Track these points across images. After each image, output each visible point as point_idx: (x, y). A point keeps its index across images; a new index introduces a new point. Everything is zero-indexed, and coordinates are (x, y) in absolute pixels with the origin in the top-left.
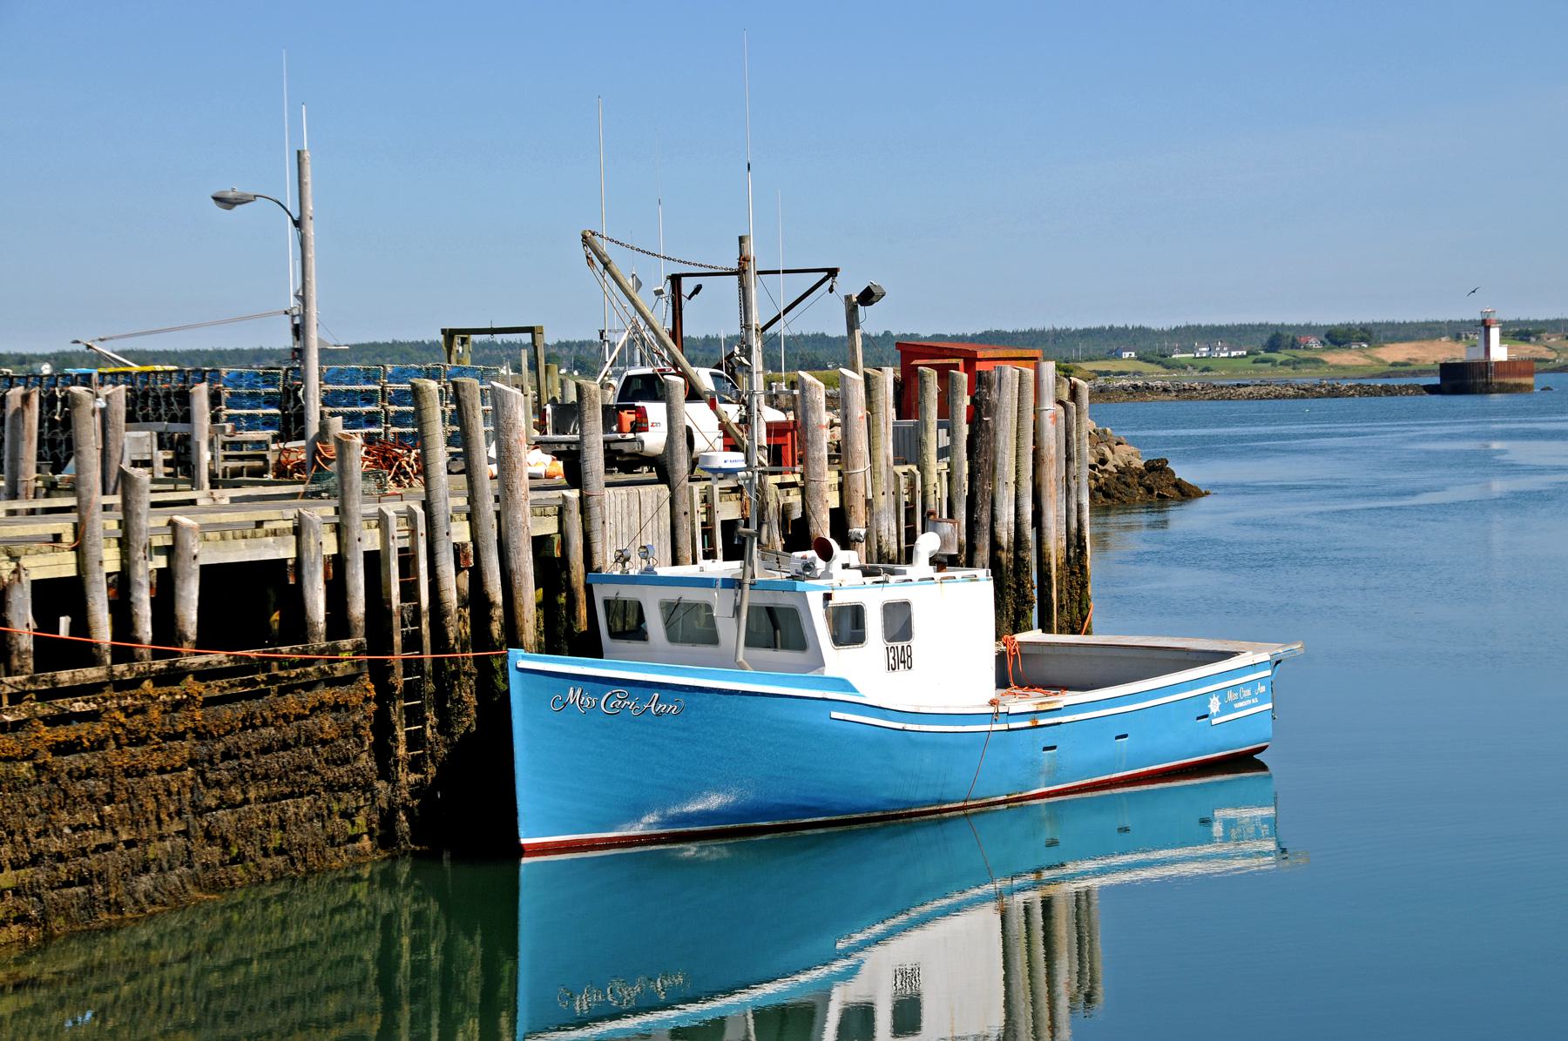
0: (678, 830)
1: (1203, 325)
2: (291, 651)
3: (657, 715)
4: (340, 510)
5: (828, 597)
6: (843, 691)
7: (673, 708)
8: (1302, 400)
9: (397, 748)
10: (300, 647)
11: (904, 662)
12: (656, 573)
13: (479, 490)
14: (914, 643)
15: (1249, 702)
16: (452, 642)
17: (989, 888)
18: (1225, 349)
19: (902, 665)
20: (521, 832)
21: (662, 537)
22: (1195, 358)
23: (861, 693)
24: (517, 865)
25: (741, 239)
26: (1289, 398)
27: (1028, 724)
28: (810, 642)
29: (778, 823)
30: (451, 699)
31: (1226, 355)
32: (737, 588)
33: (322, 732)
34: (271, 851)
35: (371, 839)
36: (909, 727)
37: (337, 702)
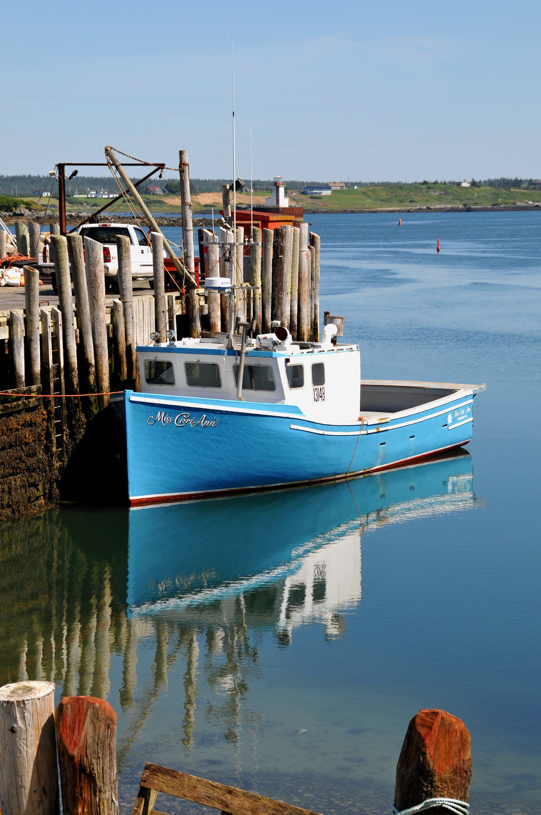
0: (209, 491)
1: (86, 177)
2: (12, 393)
3: (204, 427)
4: (27, 311)
5: (287, 360)
6: (296, 413)
7: (213, 423)
8: (173, 228)
9: (52, 447)
10: (16, 390)
11: (321, 397)
12: (176, 346)
13: (83, 299)
14: (325, 386)
15: (463, 417)
16: (76, 386)
17: (357, 522)
18: (106, 193)
19: (320, 398)
20: (130, 493)
21: (152, 326)
22: (88, 198)
23: (304, 414)
24: (128, 511)
25: (181, 153)
26: (165, 226)
27: (375, 431)
28: (277, 386)
29: (259, 487)
30: (75, 419)
31: (107, 196)
32: (237, 355)
33: (26, 438)
34: (5, 506)
35: (44, 499)
36: (326, 433)
37: (31, 421)
